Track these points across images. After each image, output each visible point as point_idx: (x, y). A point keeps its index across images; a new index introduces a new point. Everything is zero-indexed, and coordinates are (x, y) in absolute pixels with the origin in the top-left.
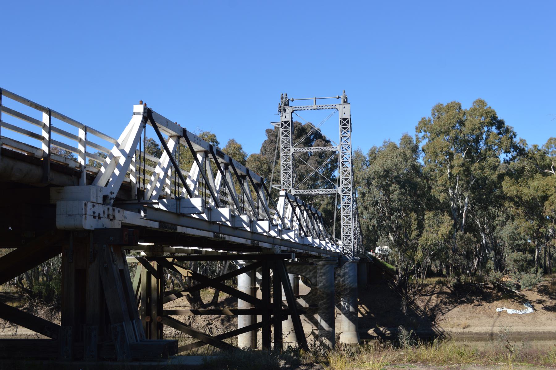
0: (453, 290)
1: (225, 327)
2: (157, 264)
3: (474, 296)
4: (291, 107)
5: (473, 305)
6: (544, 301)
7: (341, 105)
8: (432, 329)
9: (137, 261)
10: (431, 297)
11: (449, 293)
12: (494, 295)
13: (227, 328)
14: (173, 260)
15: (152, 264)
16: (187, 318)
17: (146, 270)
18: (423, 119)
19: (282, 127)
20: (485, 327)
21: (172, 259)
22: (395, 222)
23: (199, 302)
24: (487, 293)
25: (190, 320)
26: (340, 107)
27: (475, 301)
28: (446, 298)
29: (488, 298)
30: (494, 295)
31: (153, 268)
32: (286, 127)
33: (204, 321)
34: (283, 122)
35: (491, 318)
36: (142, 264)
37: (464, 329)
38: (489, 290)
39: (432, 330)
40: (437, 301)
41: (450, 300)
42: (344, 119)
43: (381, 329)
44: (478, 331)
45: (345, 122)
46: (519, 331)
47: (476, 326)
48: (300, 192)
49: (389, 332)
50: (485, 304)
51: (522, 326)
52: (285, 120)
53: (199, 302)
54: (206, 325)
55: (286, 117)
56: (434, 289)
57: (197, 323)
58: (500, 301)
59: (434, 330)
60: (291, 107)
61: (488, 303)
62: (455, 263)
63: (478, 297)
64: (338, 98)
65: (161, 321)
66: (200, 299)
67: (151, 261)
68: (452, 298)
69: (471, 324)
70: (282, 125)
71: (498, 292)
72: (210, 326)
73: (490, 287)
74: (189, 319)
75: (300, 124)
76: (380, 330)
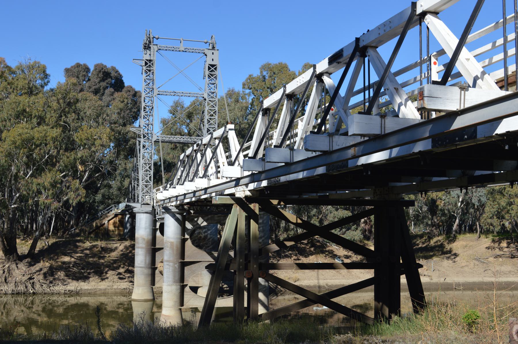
1: (48, 282)
2: (259, 208)
4: (157, 45)
6: (350, 256)
7: (209, 50)
9: (232, 202)
12: (308, 250)
13: (52, 283)
15: (252, 206)
16: (2, 272)
17: (244, 214)
18: (250, 76)
19: (145, 66)
20: (312, 280)
21: (277, 201)
22: (33, 172)
23: (15, 254)
24: (302, 248)
25: (5, 274)
26: (209, 53)
27: (292, 255)
30: (308, 250)
31: (253, 211)
32: (150, 66)
33: (24, 275)
34: (147, 60)
36: (240, 206)
38: (304, 246)
42: (213, 66)
44: (308, 284)
45: (213, 69)
46: (342, 284)
47: (304, 280)
48: (166, 138)
49: (225, 286)
51: (343, 279)
52: (149, 59)
53: (15, 254)
54: (28, 279)
55: (150, 55)
57: (14, 277)
58: (314, 256)
60: (157, 45)
64: (206, 43)
66: (15, 249)
69: (299, 277)
70: (146, 64)
71: (311, 247)
72: (32, 281)
73: (304, 243)
74: (4, 272)
75: (105, 66)
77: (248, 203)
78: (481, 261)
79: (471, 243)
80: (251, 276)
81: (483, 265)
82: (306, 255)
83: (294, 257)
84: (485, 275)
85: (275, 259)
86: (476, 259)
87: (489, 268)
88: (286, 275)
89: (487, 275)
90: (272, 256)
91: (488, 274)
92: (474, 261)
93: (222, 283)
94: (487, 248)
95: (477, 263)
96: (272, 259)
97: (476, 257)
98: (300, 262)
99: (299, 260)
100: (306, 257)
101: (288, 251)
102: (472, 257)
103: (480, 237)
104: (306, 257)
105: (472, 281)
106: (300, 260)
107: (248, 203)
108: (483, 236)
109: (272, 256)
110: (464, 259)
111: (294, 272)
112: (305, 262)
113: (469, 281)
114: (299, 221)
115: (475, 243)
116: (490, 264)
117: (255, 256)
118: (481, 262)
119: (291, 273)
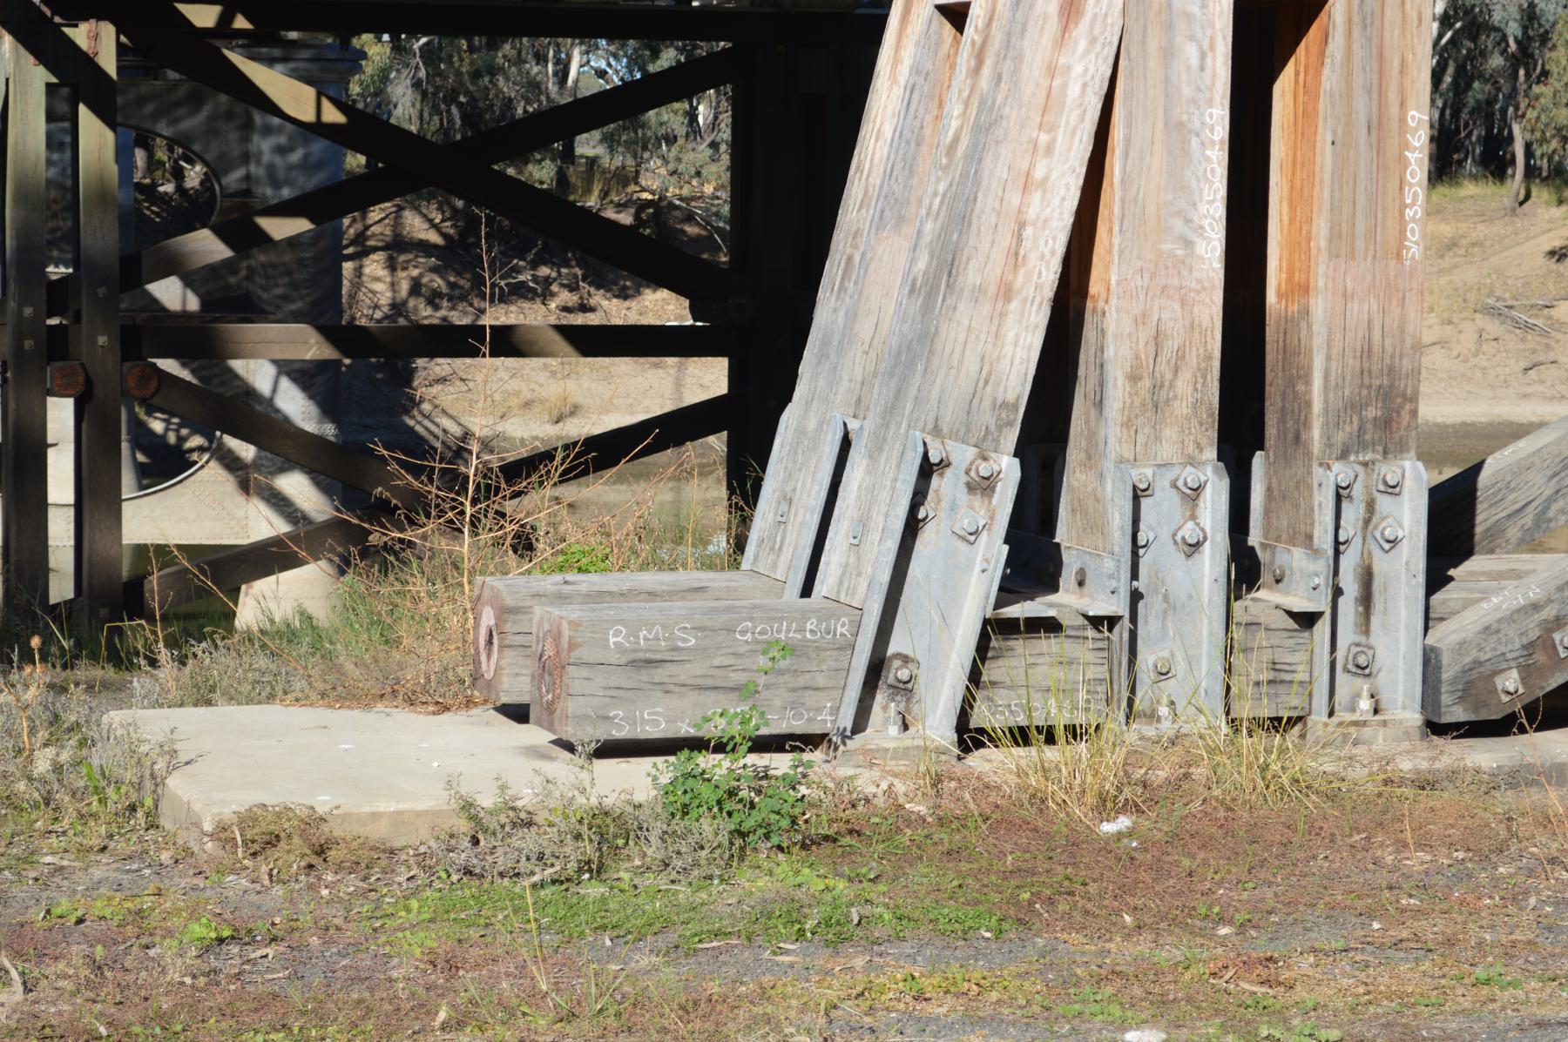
0: (452, 231)
2: (119, 44)
3: (545, 264)
5: (553, 305)
8: (411, 423)
10: (361, 267)
11: (436, 246)
14: (225, 19)
15: (80, 34)
17: (39, 76)
27: (555, 288)
28: (434, 270)
29: (611, 276)
31: (87, 62)
35: (654, 371)
37: (557, 422)
39: (411, 429)
40: (393, 286)
41: (452, 279)
43: (157, 426)
47: (607, 411)
50: (605, 303)
56: (367, 228)
59: (418, 428)
61: (615, 296)
62: (528, 102)
63: (564, 271)
65: (153, 395)
67: (74, 19)
68: (459, 274)
69: (581, 400)
76: (151, 433)
77: (57, 19)
78: (1513, 319)
79: (1481, 227)
80: (81, 379)
81: (1523, 340)
82: (625, 288)
83: (566, 297)
84: (1529, 390)
85: (461, 306)
86: (1491, 311)
87: (1552, 356)
88: (513, 385)
89: (1538, 388)
90: (445, 289)
91: (1542, 382)
92: (1482, 321)
93: (181, 426)
94: (1552, 253)
95: (1492, 327)
96: (445, 303)
97: (1491, 301)
98: (593, 319)
99: (585, 308)
100: (624, 295)
101: (534, 265)
102: (1471, 297)
103: (1528, 197)
104: (626, 298)
105: (1459, 420)
106: (592, 310)
107: (57, 19)
108: (1541, 194)
109: (445, 289)
110: (1432, 310)
111: (553, 373)
112: (617, 321)
113: (1439, 420)
114: (332, 115)
115: (1497, 228)
116: (1559, 336)
117: (101, 291)
118: (1517, 324)
119: (542, 377)
